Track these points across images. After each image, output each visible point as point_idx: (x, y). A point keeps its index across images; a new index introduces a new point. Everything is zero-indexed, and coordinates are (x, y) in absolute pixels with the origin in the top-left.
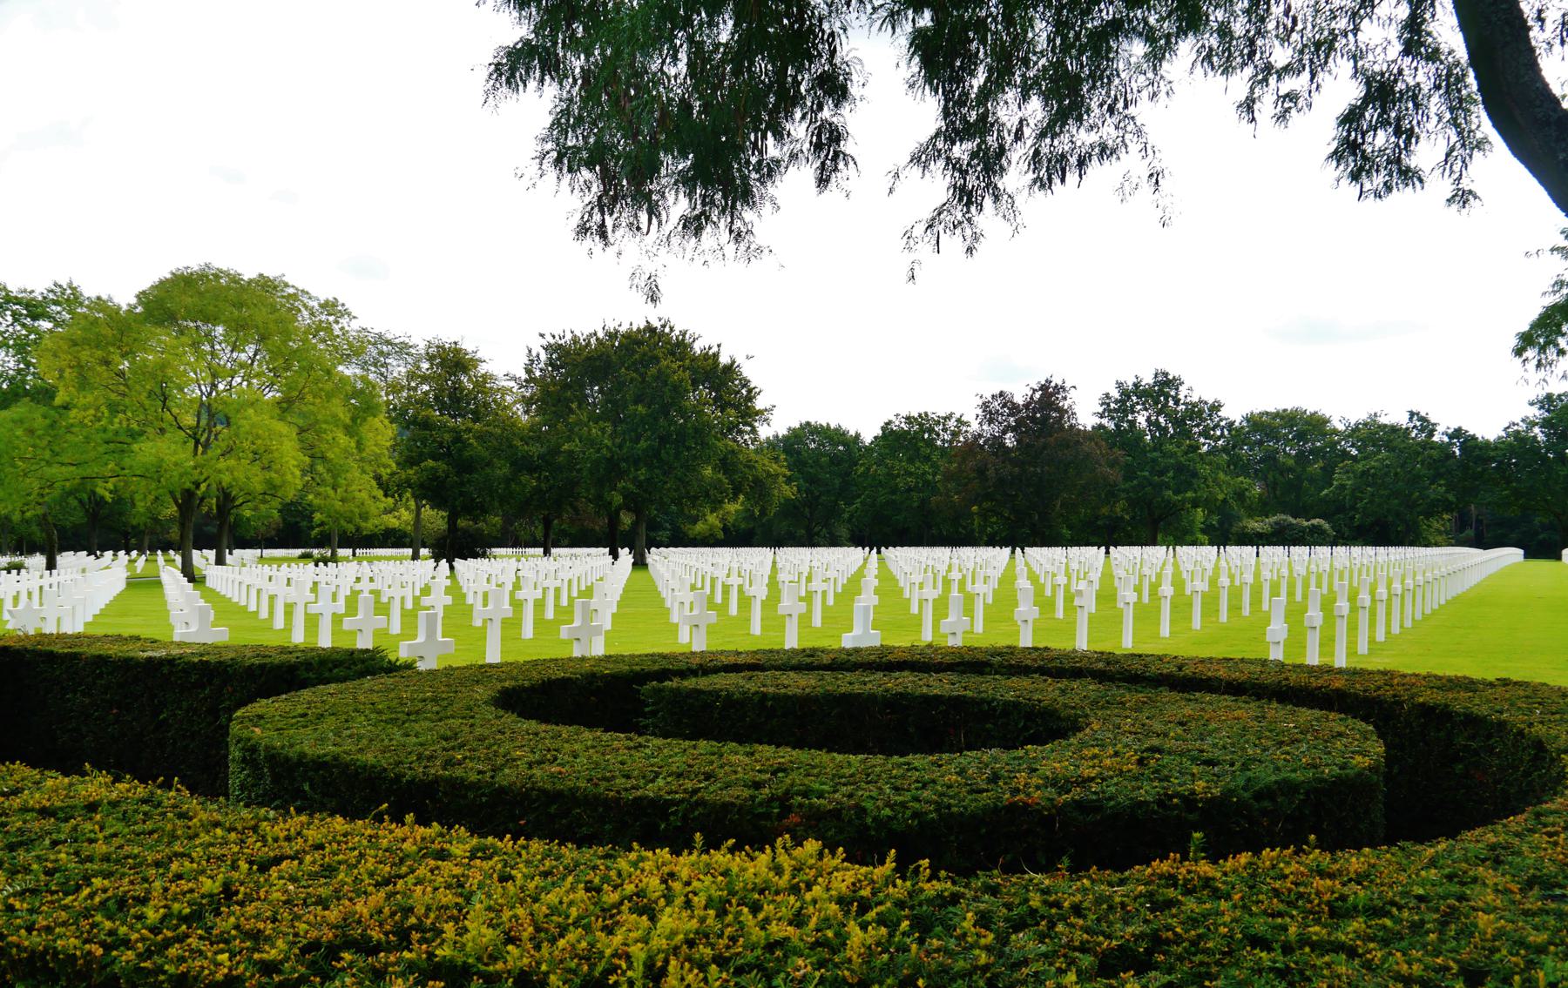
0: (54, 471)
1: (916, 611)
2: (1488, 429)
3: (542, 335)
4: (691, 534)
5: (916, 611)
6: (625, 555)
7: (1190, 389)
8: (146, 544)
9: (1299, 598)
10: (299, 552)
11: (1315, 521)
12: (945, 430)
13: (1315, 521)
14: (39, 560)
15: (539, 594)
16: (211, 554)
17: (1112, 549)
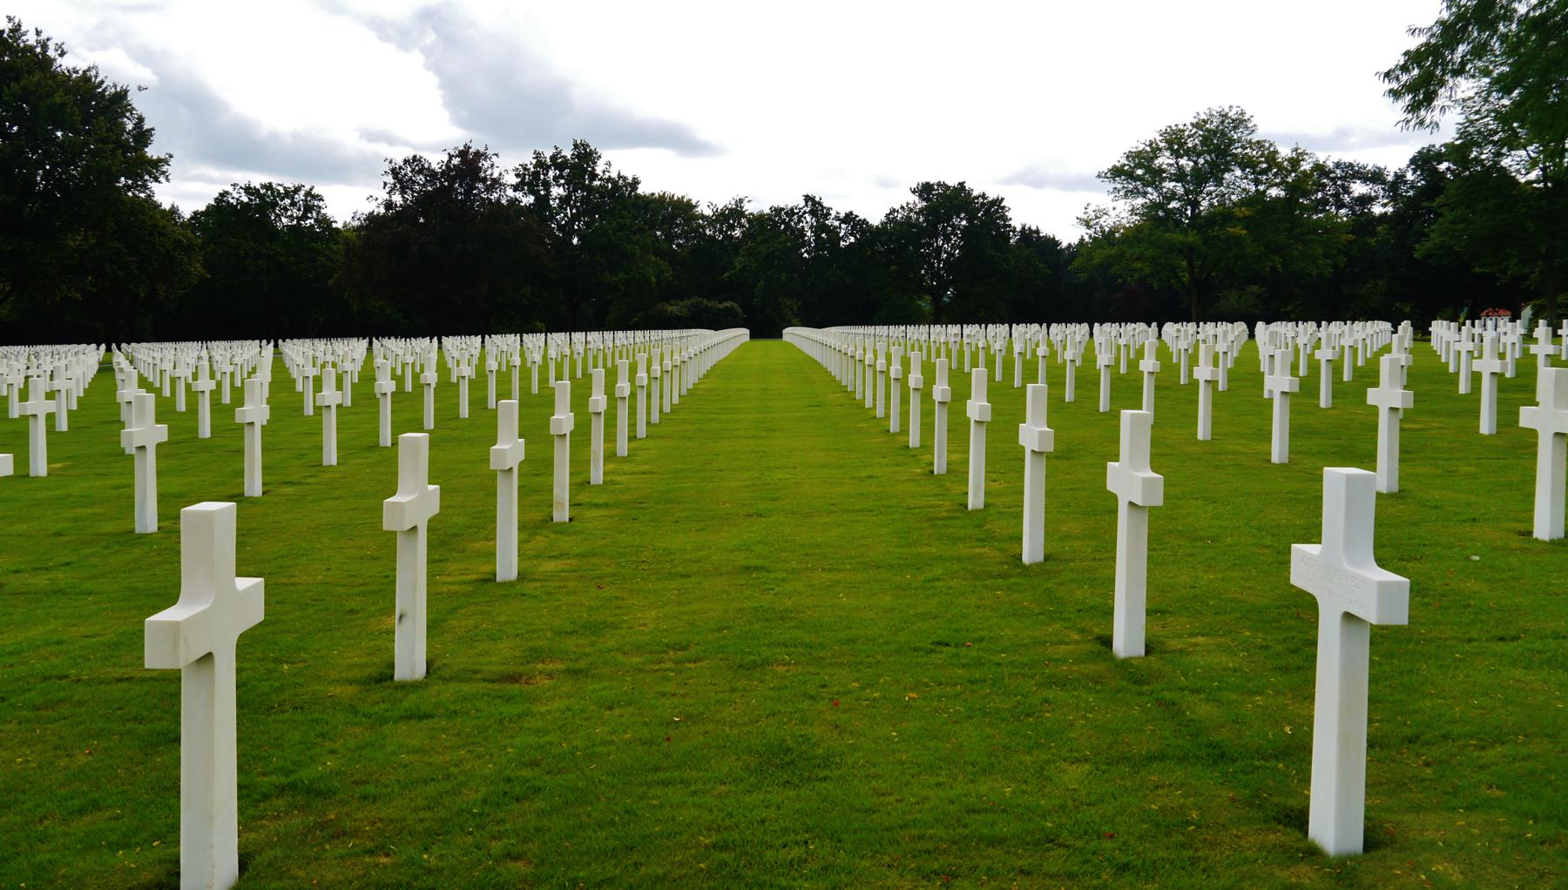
2: (875, 216)
6: (1406, 327)
11: (728, 304)
12: (293, 204)
13: (728, 304)
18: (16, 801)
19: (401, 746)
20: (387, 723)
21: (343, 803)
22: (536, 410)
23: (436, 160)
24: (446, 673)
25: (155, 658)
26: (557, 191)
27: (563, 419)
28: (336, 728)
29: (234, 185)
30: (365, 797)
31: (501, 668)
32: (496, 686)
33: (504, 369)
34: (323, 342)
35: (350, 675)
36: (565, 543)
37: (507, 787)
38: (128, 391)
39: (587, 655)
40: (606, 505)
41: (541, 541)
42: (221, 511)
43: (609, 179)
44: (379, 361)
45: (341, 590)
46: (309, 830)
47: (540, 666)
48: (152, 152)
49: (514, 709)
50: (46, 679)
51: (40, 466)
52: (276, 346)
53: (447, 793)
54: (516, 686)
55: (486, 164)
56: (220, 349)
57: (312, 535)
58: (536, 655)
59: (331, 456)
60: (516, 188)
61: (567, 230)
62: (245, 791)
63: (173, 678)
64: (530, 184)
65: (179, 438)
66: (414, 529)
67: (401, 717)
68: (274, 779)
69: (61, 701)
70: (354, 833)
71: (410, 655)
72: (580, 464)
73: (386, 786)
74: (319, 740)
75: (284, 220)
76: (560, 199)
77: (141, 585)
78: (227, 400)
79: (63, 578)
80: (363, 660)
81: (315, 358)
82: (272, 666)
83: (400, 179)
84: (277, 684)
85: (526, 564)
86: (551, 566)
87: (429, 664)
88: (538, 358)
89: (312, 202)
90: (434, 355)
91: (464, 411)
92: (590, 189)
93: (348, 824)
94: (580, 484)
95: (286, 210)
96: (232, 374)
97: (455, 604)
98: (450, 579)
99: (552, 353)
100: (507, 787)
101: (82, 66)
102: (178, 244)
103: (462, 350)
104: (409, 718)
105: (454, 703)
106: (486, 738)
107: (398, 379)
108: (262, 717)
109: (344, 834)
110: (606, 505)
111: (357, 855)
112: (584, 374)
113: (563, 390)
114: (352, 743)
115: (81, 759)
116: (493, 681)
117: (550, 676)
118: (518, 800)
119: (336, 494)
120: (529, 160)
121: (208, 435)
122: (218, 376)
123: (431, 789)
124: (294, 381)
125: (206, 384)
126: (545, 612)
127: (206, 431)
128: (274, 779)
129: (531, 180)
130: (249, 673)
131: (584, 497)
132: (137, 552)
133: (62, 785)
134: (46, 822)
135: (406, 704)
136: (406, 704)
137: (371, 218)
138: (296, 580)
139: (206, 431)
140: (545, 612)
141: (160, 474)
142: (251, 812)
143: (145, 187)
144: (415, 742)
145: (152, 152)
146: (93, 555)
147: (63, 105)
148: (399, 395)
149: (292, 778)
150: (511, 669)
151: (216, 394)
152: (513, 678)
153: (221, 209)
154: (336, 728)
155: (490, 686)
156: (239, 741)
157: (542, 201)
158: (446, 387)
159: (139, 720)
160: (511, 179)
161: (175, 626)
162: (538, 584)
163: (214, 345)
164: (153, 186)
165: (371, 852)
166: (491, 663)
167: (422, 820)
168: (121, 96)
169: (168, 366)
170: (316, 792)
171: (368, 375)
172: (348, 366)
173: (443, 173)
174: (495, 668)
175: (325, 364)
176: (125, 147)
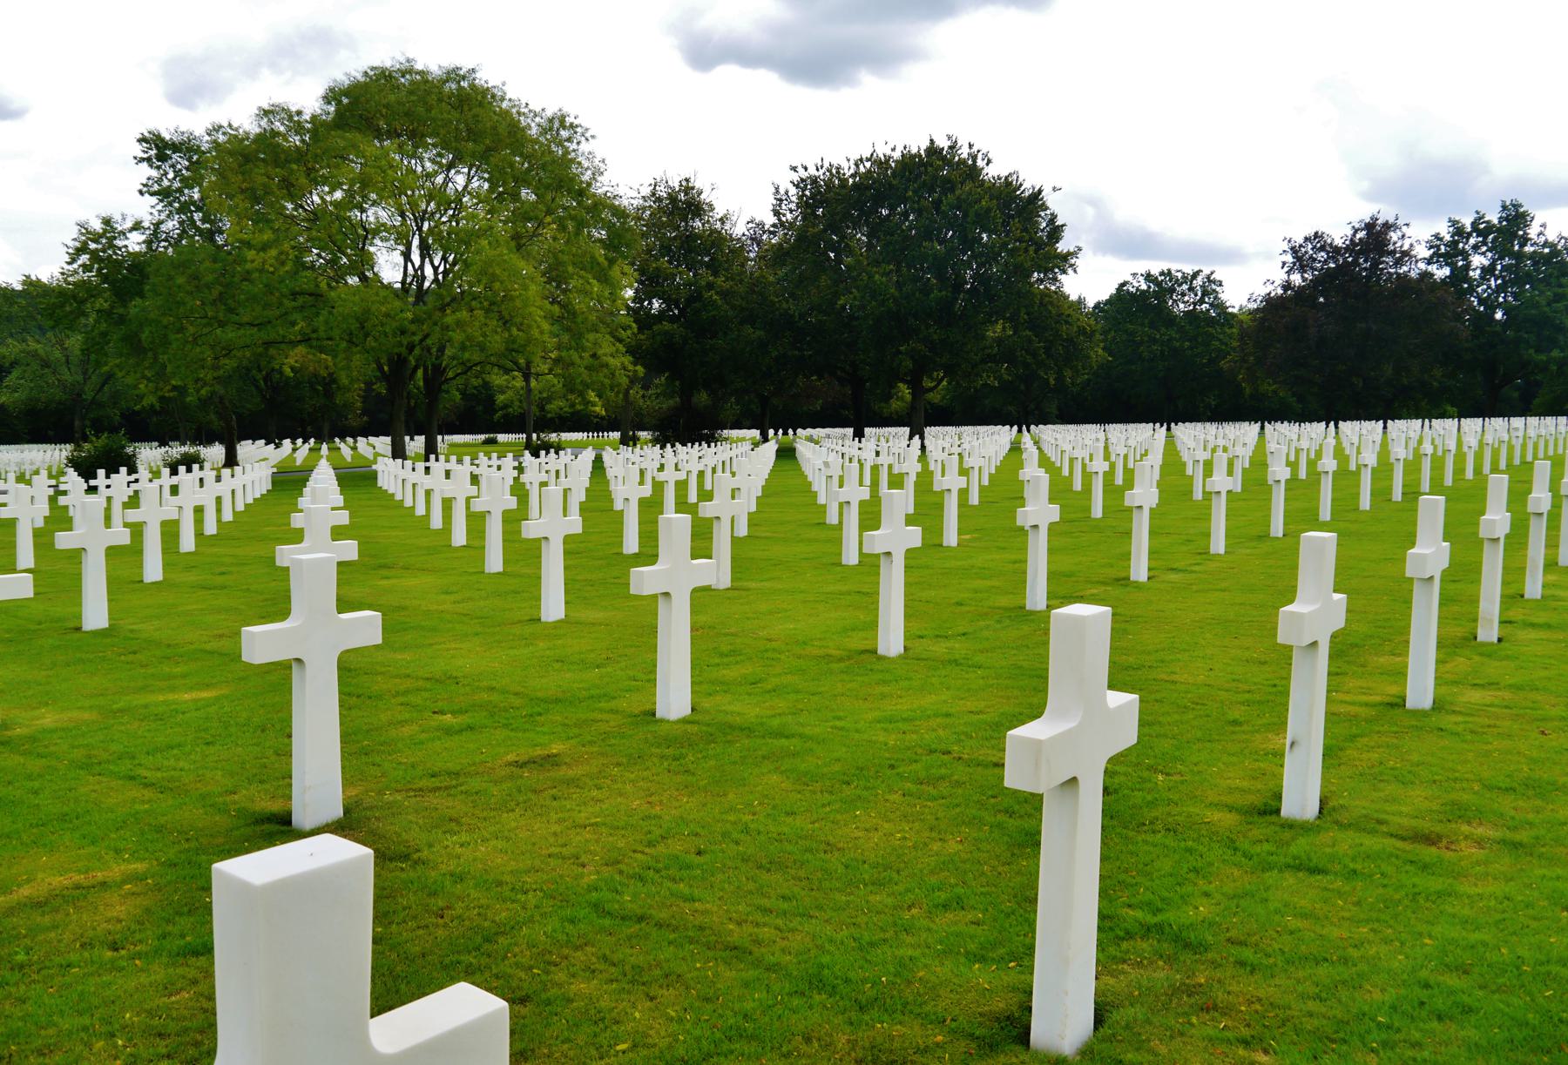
0: (230, 334)
1: (835, 521)
3: (794, 169)
4: (886, 412)
5: (835, 521)
7: (1544, 226)
8: (326, 431)
9: (1469, 474)
10: (483, 437)
12: (1191, 289)
14: (216, 452)
15: (646, 490)
16: (383, 443)
17: (1341, 424)
18: (891, 880)
19: (1286, 905)
20: (1271, 868)
21: (1215, 965)
22: (1465, 505)
23: (1339, 234)
24: (1344, 817)
25: (1015, 778)
26: (1478, 261)
27: (1496, 519)
28: (1211, 864)
29: (1134, 275)
30: (1241, 963)
31: (1414, 823)
32: (1407, 846)
33: (1440, 453)
34: (1215, 425)
35: (1229, 799)
36: (1493, 669)
37: (1423, 994)
38: (1032, 471)
39: (1531, 824)
40: (1548, 626)
41: (1461, 663)
42: (1094, 616)
43: (1546, 244)
44: (1272, 446)
45: (1223, 695)
46: (1175, 991)
47: (1465, 828)
48: (1062, 247)
49: (1435, 884)
50: (932, 752)
51: (951, 538)
52: (1169, 429)
53: (1344, 982)
54: (1433, 849)
55: (1394, 236)
56: (1116, 431)
57: (1200, 704)
58: (1459, 812)
59: (1218, 545)
60: (1429, 262)
61: (1490, 304)
62: (1106, 920)
63: (1034, 802)
64: (1446, 255)
65: (1073, 516)
66: (1314, 644)
67: (1288, 866)
68: (1139, 914)
69: (942, 778)
70: (1226, 1011)
71: (1301, 793)
72: (1514, 572)
73: (1268, 956)
74: (1192, 876)
75: (1182, 306)
76: (1483, 269)
77: (1025, 664)
78: (1119, 481)
79: (959, 648)
80: (1245, 784)
81: (1206, 442)
82: (1146, 774)
83: (1300, 260)
84: (1149, 798)
85: (1443, 690)
86: (1476, 696)
87: (1323, 802)
88: (1474, 443)
89: (1210, 287)
90: (1331, 441)
91: (1365, 503)
92: (1519, 256)
93: (1220, 996)
94: (1513, 597)
95: (1183, 295)
96: (1126, 456)
97: (1354, 730)
98: (1348, 698)
99: (1489, 438)
100: (1423, 994)
101: (1004, 174)
102: (1082, 331)
103: (1362, 435)
104: (1299, 868)
105: (1353, 860)
106: (1395, 917)
107: (1293, 465)
108: (1131, 834)
109: (1215, 1008)
110: (1548, 626)
111: (1229, 1041)
112: (1524, 463)
113: (1499, 486)
114: (1229, 888)
115: (953, 846)
116: (1403, 839)
117: (1480, 843)
118: (1440, 1018)
119: (1223, 585)
120: (1446, 234)
121: (1099, 515)
122: (1113, 458)
123: (1323, 971)
124: (1184, 464)
125: (1100, 466)
126: (1470, 756)
127: (1097, 512)
128: (1139, 914)
129: (1450, 251)
130: (1122, 778)
131: (1516, 614)
132: (1026, 628)
133: (932, 872)
134: (914, 911)
135: (1293, 850)
136: (1293, 850)
137: (1269, 300)
138: (1174, 677)
139: (1097, 512)
140: (1470, 756)
141: (1051, 551)
142: (1112, 950)
143: (1055, 279)
144: (1304, 903)
145: (1062, 247)
146: (987, 627)
147: (989, 210)
148: (1293, 482)
149: (1159, 918)
150: (1425, 826)
151: (1109, 475)
152: (1430, 840)
153: (1123, 299)
154: (1211, 864)
155: (1400, 844)
156: (1104, 859)
157: (1459, 275)
158: (1346, 477)
159: (1011, 813)
160: (1423, 252)
161: (1036, 745)
162: (1460, 719)
163: (1111, 427)
164: (1062, 277)
165: (1246, 1043)
166: (1400, 814)
167: (1311, 1015)
168: (1037, 195)
169: (1067, 447)
170: (1185, 943)
171: (1260, 461)
172: (1239, 451)
173: (1347, 249)
174: (1405, 821)
175: (1217, 448)
176: (1039, 245)
